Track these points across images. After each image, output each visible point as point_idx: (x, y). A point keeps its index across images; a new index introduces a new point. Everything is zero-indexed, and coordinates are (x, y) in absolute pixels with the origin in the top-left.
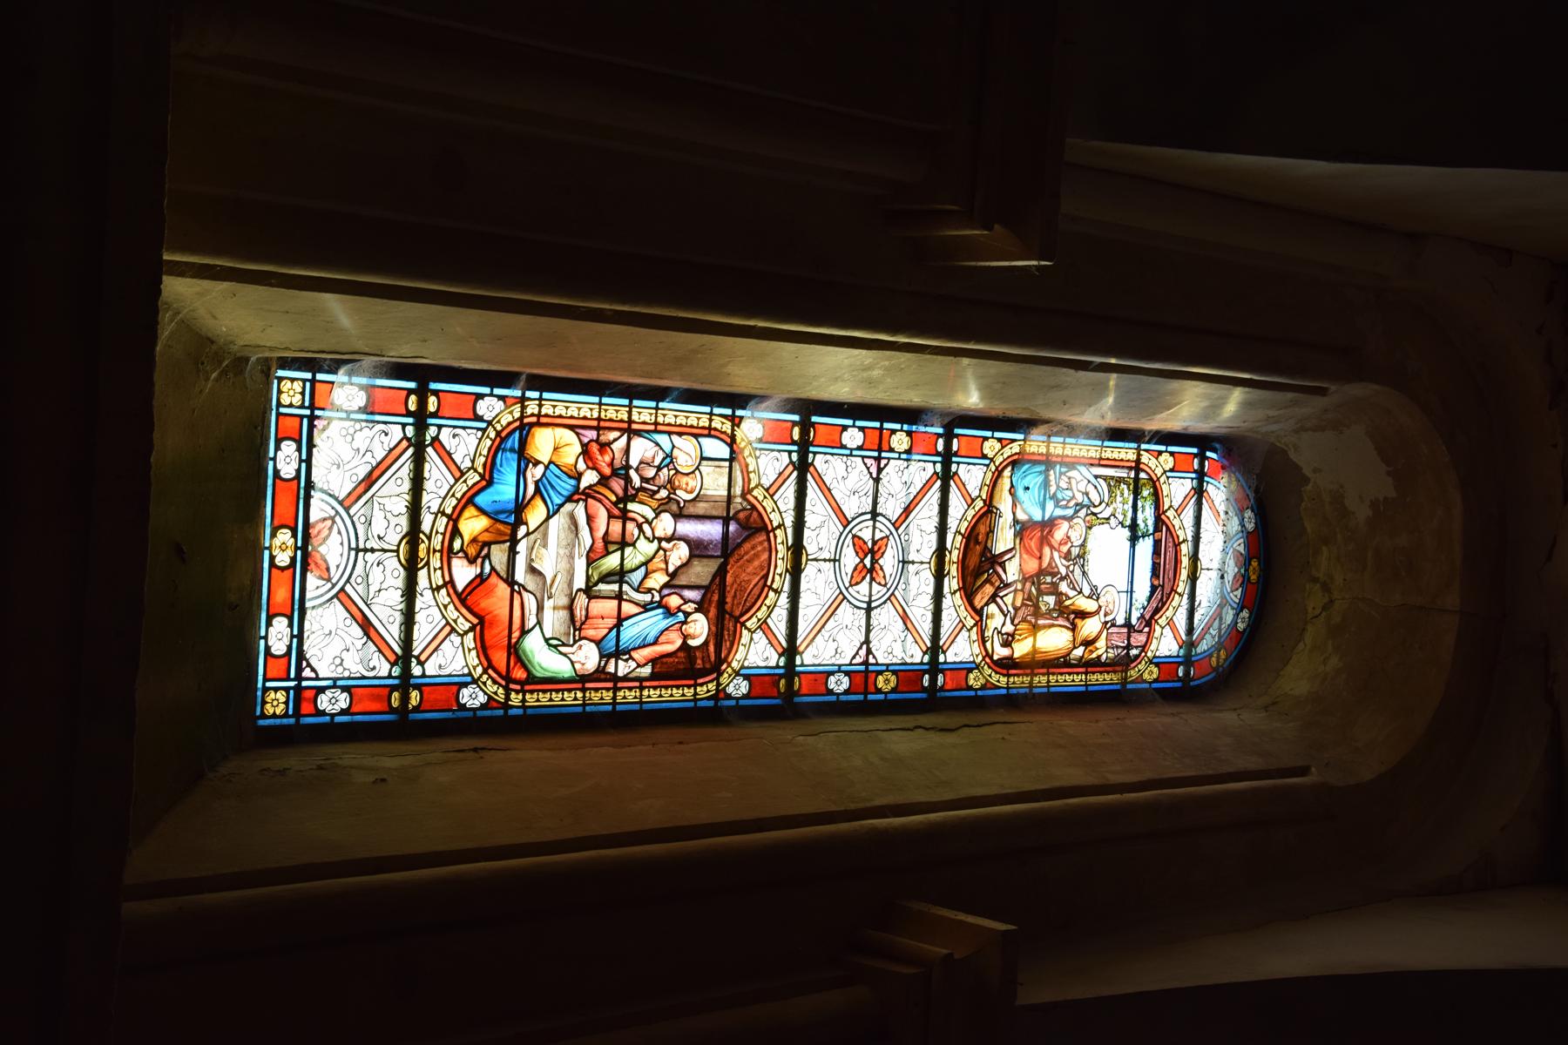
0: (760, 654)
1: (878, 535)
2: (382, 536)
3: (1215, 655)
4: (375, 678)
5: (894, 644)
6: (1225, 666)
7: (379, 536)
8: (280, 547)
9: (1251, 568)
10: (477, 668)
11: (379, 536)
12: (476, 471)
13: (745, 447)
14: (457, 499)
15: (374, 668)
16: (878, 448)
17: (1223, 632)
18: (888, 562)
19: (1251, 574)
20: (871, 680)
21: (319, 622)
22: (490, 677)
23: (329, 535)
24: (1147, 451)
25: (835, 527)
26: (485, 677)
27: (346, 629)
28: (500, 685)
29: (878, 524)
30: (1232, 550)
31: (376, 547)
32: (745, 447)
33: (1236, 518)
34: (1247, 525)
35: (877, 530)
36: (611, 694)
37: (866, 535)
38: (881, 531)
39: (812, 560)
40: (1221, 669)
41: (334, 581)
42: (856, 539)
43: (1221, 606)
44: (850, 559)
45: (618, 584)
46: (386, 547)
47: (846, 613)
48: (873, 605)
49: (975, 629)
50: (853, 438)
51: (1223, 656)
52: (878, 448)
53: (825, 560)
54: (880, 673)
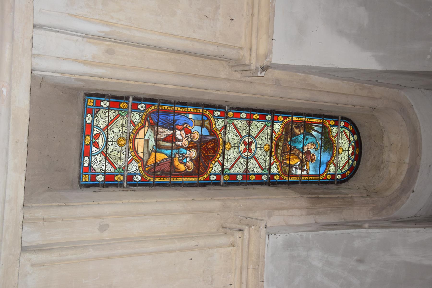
0: (275, 126)
1: (250, 140)
2: (112, 138)
3: (347, 173)
4: (111, 173)
5: (241, 125)
6: (350, 175)
7: (112, 138)
8: (88, 140)
9: (357, 150)
10: (142, 172)
11: (112, 138)
12: (141, 123)
13: (281, 173)
14: (136, 130)
15: (111, 170)
16: (249, 120)
17: (349, 166)
18: (253, 147)
19: (357, 152)
20: (248, 177)
21: (96, 159)
22: (327, 126)
23: (99, 137)
24: (325, 120)
25: (239, 138)
26: (328, 126)
27: (103, 160)
28: (324, 123)
29: (250, 138)
30: (351, 145)
31: (111, 140)
32: (281, 173)
33: (352, 137)
34: (355, 139)
35: (250, 139)
36: (306, 120)
37: (247, 140)
38: (251, 139)
39: (344, 150)
40: (348, 176)
41: (100, 149)
42: (251, 152)
43: (348, 160)
44: (243, 147)
45: (171, 150)
46: (114, 140)
47: (242, 160)
48: (249, 158)
49: (279, 165)
50: (243, 115)
51: (349, 173)
52: (249, 120)
53: (346, 150)
54: (251, 175)
